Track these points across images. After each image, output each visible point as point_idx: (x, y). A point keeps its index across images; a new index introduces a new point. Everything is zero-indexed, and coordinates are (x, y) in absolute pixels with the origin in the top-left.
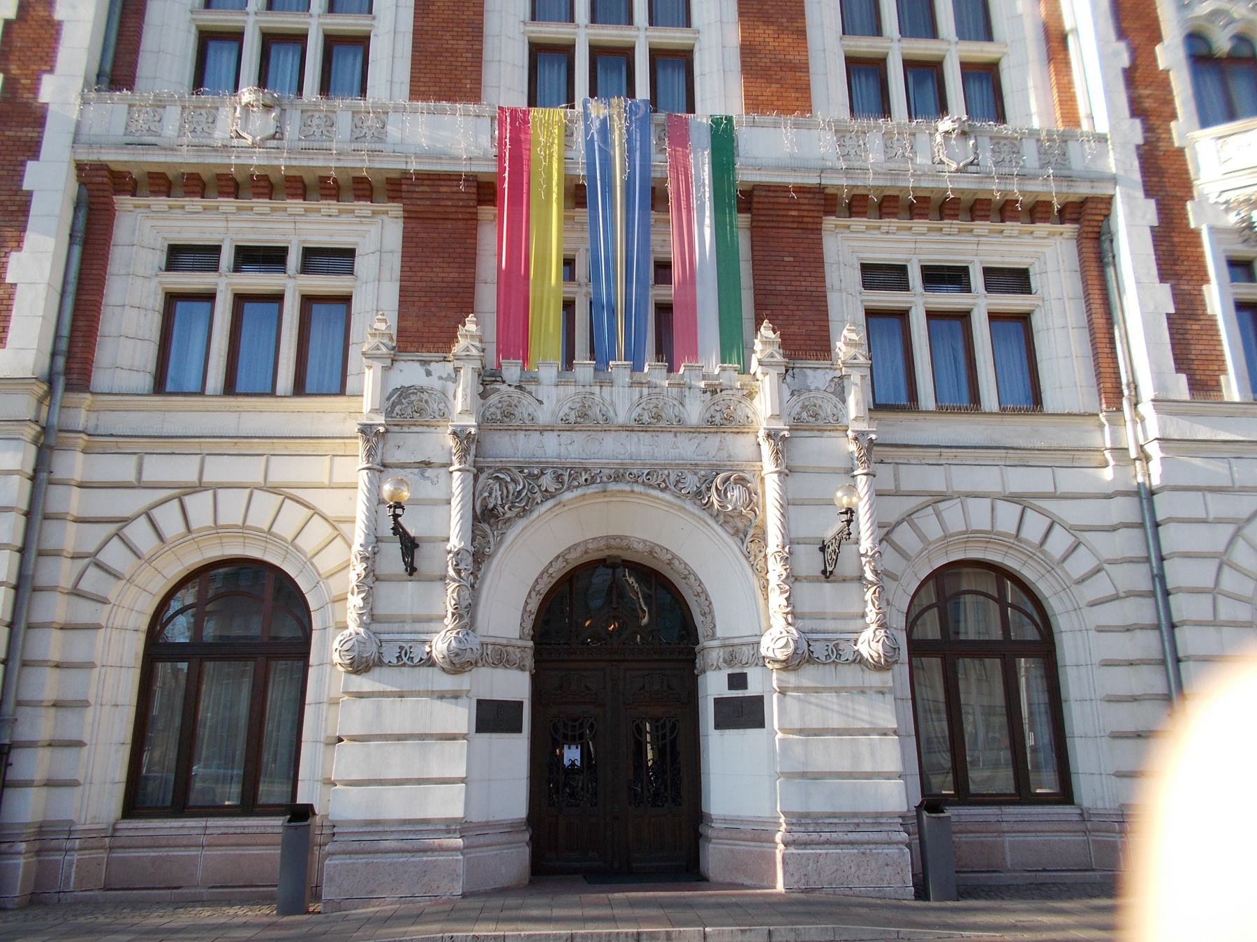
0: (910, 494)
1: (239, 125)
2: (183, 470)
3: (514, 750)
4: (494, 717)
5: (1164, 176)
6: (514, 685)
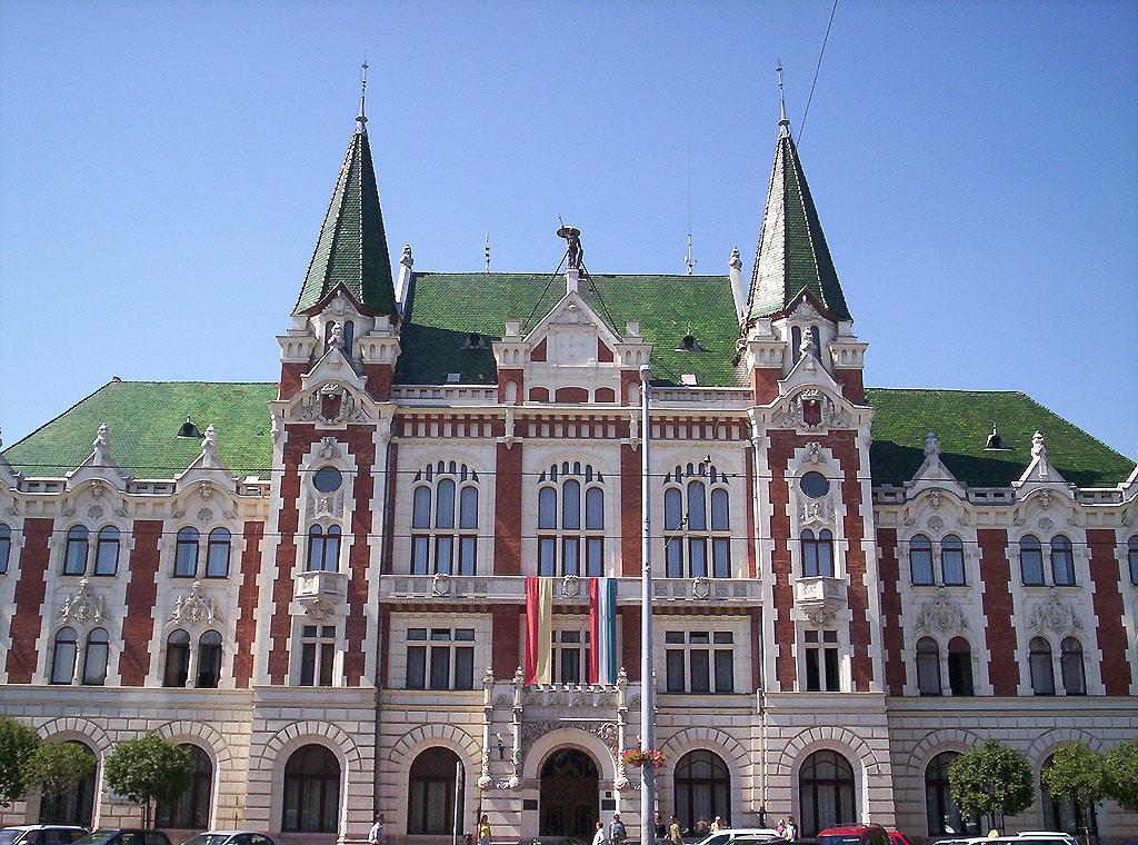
0: (286, 720)
1: (433, 590)
2: (419, 717)
3: (535, 815)
4: (529, 805)
5: (783, 597)
6: (535, 795)
